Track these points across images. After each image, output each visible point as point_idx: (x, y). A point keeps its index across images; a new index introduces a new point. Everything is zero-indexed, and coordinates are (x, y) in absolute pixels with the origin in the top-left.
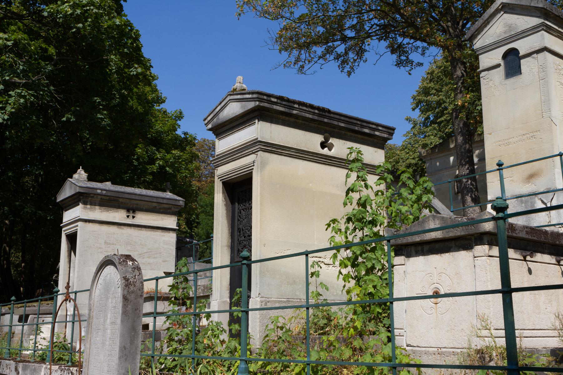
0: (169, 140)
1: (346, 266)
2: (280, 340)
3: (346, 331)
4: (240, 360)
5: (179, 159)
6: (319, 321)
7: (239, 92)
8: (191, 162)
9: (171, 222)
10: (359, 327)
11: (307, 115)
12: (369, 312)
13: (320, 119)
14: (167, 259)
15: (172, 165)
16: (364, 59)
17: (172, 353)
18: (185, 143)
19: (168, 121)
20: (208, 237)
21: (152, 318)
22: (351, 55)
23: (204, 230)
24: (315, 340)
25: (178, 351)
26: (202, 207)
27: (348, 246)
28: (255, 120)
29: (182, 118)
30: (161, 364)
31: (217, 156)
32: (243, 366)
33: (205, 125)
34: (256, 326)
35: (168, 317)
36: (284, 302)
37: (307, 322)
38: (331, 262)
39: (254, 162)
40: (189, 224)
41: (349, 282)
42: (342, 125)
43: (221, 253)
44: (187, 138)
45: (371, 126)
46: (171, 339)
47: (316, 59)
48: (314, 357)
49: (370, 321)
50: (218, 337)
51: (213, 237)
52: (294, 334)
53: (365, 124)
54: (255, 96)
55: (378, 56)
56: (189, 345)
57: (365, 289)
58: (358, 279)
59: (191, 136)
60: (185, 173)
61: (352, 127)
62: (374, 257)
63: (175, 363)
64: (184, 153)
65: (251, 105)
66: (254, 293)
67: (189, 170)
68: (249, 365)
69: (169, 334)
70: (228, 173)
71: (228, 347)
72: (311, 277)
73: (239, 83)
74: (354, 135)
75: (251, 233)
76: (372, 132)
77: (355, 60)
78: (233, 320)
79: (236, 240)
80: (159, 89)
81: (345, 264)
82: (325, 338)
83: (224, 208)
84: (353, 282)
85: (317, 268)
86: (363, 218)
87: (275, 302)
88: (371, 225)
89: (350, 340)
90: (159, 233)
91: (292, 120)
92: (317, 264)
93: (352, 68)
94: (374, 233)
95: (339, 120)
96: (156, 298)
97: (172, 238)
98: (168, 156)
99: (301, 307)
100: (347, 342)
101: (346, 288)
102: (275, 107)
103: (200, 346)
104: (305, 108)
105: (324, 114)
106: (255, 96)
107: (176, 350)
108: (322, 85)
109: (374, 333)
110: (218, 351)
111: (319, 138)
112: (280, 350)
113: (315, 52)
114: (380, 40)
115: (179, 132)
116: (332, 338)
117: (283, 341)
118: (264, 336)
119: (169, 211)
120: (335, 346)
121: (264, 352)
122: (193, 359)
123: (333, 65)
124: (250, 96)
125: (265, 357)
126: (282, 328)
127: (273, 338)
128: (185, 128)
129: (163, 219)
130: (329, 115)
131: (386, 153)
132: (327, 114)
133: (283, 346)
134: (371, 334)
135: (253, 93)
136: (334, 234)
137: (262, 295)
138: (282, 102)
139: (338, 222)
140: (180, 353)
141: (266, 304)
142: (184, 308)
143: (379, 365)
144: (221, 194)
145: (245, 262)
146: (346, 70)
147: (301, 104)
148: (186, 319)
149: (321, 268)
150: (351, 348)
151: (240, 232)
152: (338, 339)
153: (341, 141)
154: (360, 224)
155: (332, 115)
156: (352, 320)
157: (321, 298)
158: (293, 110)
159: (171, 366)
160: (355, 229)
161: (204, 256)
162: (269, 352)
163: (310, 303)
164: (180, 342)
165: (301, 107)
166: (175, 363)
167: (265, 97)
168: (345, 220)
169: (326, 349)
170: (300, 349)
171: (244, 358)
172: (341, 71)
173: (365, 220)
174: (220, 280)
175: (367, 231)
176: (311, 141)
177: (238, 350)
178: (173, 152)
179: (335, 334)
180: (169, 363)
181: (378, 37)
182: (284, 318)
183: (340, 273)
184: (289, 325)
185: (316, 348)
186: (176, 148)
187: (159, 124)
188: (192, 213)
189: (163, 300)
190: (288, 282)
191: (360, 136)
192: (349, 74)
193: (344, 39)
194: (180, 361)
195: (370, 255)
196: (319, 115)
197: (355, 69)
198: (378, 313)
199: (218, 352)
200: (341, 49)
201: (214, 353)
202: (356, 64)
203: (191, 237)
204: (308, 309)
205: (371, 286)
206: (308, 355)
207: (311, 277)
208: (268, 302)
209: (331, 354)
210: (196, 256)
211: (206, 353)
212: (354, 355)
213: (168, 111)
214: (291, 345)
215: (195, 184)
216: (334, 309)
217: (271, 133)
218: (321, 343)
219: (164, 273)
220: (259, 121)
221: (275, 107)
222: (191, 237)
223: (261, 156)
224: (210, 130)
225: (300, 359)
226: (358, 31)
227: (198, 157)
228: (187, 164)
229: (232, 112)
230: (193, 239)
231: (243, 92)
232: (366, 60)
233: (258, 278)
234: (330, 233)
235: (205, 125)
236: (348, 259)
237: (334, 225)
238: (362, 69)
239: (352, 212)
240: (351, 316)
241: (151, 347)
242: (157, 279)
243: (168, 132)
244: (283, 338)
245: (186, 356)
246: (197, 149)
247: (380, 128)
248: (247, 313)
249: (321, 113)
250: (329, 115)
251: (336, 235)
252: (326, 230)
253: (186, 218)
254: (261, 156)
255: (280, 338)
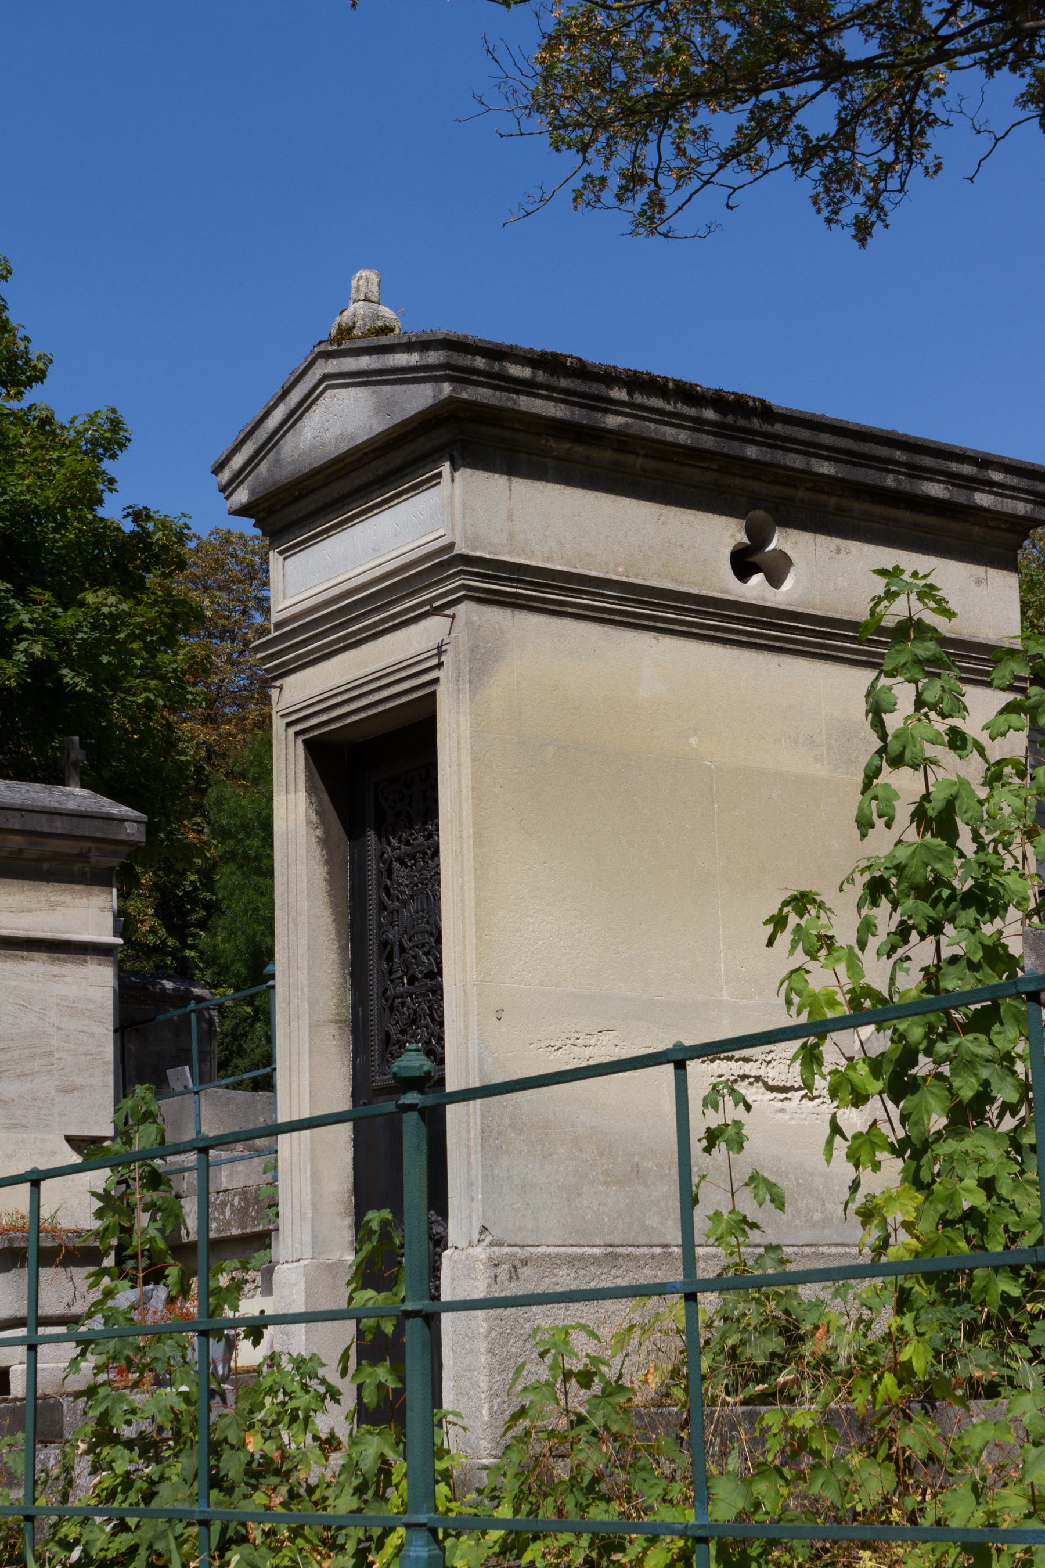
0: (69, 546)
1: (859, 1099)
2: (582, 1431)
3: (865, 1386)
4: (408, 1526)
5: (114, 629)
6: (743, 1343)
7: (364, 343)
8: (169, 641)
9: (88, 914)
10: (918, 1365)
11: (669, 433)
12: (967, 1297)
13: (728, 447)
14: (78, 1081)
15: (87, 659)
16: (929, 159)
17: (112, 1495)
18: (140, 555)
19: (59, 461)
20: (257, 966)
21: (21, 1351)
22: (868, 143)
23: (241, 939)
24: (734, 1427)
25: (139, 1484)
26: (223, 834)
27: (867, 1008)
28: (437, 463)
29: (122, 446)
30: (68, 1546)
31: (279, 625)
32: (420, 1550)
33: (223, 489)
34: (474, 1378)
35: (85, 1343)
36: (595, 1260)
37: (692, 1350)
38: (794, 1075)
39: (440, 650)
40: (173, 910)
41: (877, 1166)
42: (827, 468)
43: (311, 1061)
44: (149, 535)
45: (955, 467)
46: (105, 1435)
47: (708, 167)
48: (726, 1505)
49: (971, 1335)
50: (307, 1419)
51: (272, 977)
52: (638, 1400)
53: (927, 461)
54: (434, 357)
55: (985, 142)
56: (183, 1458)
57: (951, 1198)
58: (914, 1149)
59: (164, 525)
60: (145, 692)
61: (868, 476)
62: (987, 1051)
63: (125, 1540)
64: (139, 602)
65: (418, 398)
66: (456, 1230)
67: (164, 679)
68: (449, 1543)
69: (94, 1413)
70: (326, 702)
71: (351, 1467)
72: (708, 1150)
73: (364, 298)
74: (877, 509)
75: (439, 963)
76: (961, 497)
77: (886, 169)
78: (373, 1347)
79: (374, 993)
80: (13, 323)
81: (854, 1091)
82: (771, 1416)
83: (318, 854)
84: (893, 1167)
85: (731, 1112)
86: (939, 881)
87: (553, 1262)
88: (972, 912)
89: (885, 1424)
90: (36, 968)
91: (605, 455)
92: (732, 1091)
93: (873, 202)
94: (985, 948)
95: (812, 450)
96: (32, 1255)
97: (96, 985)
98: (68, 619)
99: (660, 1290)
100: (871, 1434)
101: (860, 1197)
102: (525, 403)
103: (232, 1466)
104: (657, 402)
105: (741, 422)
106: (434, 357)
107: (127, 1481)
108: (741, 289)
109: (992, 1391)
110: (313, 1481)
111: (725, 533)
112: (581, 1471)
113: (705, 133)
114: (991, 67)
115: (112, 510)
116: (804, 1417)
117: (595, 1433)
118: (507, 1416)
119: (77, 867)
120: (816, 1454)
121: (510, 1485)
122: (205, 1523)
123: (785, 192)
124: (412, 359)
125: (516, 1511)
126: (586, 1378)
127: (550, 1423)
128: (135, 489)
129: (53, 907)
130: (767, 428)
131: (1028, 587)
132: (756, 423)
133: (593, 1458)
134: (977, 1396)
135: (424, 345)
136: (800, 958)
137: (497, 1233)
138: (553, 381)
139: (821, 905)
140: (149, 1497)
141: (514, 1274)
142: (160, 1293)
143: (1014, 1536)
144: (302, 795)
145: (412, 1098)
146: (847, 214)
147: (636, 382)
148: (168, 1348)
149: (748, 1107)
150: (889, 1457)
151: (389, 959)
152: (829, 1420)
153: (821, 539)
154: (925, 908)
155: (779, 428)
156: (895, 1339)
157: (754, 1236)
158: (606, 411)
159: (111, 1554)
160: (903, 932)
161: (241, 1052)
162: (534, 1482)
163: (701, 1275)
164: (146, 1447)
165: (638, 399)
166: (125, 1540)
167: (480, 362)
168: (857, 890)
169: (778, 1471)
170: (667, 1467)
171: (422, 1519)
172: (829, 221)
173: (946, 893)
174: (312, 1182)
175: (954, 941)
176: (691, 546)
177: (395, 1479)
178: (90, 598)
179: (820, 1398)
180: (101, 1541)
181: (982, 54)
182: (593, 1335)
183: (836, 1129)
184: (617, 1361)
185: (734, 1463)
186: (99, 582)
187: (22, 477)
188: (179, 866)
189: (65, 1264)
190: (606, 1173)
191: (906, 515)
192: (863, 231)
193: (835, 70)
194: (147, 1533)
195: (971, 1043)
196: (720, 430)
197: (888, 206)
198: (1005, 1297)
199: (311, 1490)
200: (820, 114)
201: (293, 1495)
202: (894, 183)
203: (184, 971)
204: (691, 1298)
205: (971, 1183)
206: (702, 1495)
207: (708, 1150)
208: (525, 1262)
209: (802, 1486)
210: (203, 1056)
211: (259, 1498)
212: (903, 1489)
213: (61, 418)
214: (629, 1455)
215: (193, 733)
216: (807, 1292)
217: (511, 517)
218: (759, 1442)
219: (73, 1141)
220: (454, 468)
221: (525, 403)
222: (184, 971)
223: (469, 623)
224: (243, 511)
225: (666, 1515)
226: (892, 34)
227: (200, 616)
228: (152, 650)
229: (336, 431)
230: (191, 980)
231: (380, 340)
232: (938, 167)
233: (476, 1158)
234: (785, 956)
235: (223, 489)
236: (876, 1066)
237: (803, 922)
238: (919, 203)
239: (891, 856)
240: (886, 1320)
241: (20, 1469)
242: (35, 1179)
243: (62, 510)
244: (595, 1423)
245: (172, 1517)
246: (194, 579)
247: (997, 476)
248: (431, 1321)
249: (730, 419)
250: (767, 428)
251: (811, 965)
252: (770, 943)
253: (156, 887)
254: (469, 623)
255: (581, 1420)
